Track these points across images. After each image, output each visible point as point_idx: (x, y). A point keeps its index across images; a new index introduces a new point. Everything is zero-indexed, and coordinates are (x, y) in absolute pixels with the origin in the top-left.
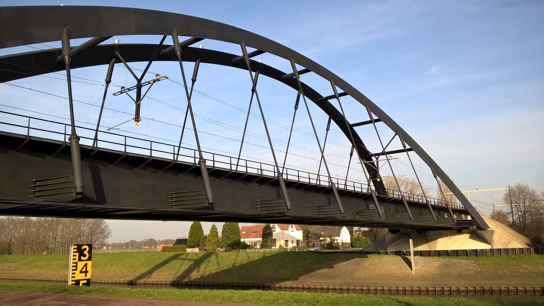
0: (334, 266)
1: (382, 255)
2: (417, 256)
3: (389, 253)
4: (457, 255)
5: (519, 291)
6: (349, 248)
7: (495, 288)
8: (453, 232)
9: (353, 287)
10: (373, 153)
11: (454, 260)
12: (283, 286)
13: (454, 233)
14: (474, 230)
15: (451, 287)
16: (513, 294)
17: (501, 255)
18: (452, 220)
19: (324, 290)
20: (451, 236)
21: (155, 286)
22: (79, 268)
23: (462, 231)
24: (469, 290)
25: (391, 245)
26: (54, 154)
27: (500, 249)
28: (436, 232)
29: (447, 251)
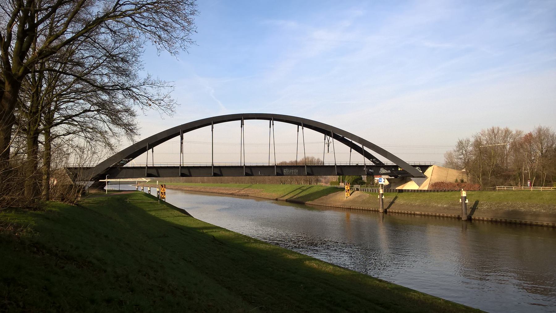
22: (162, 190)
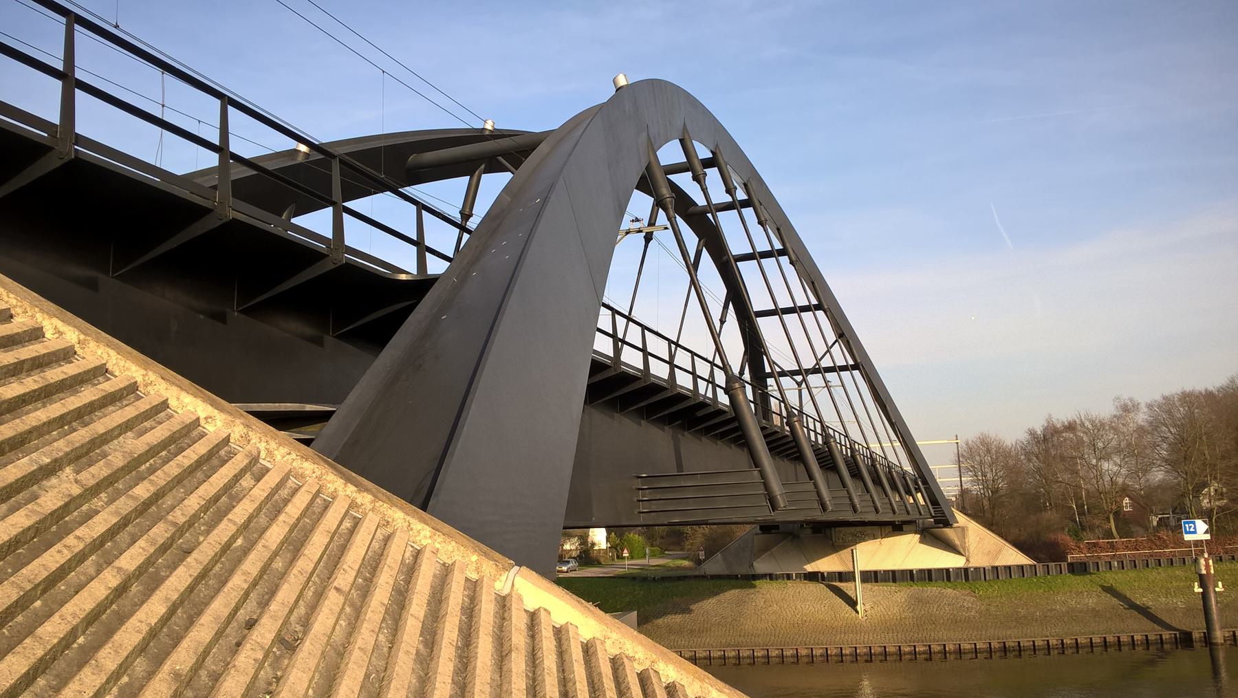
0: (693, 607)
1: (779, 581)
2: (850, 581)
3: (794, 578)
4: (930, 579)
5: (1110, 645)
6: (613, 560)
7: (1025, 643)
8: (885, 531)
9: (777, 652)
10: (786, 370)
11: (931, 590)
13: (887, 532)
14: (926, 526)
15: (753, 650)
16: (1056, 652)
17: (1011, 577)
18: (848, 501)
20: (882, 538)
23: (904, 529)
24: (980, 649)
26: (600, 399)
27: (1009, 567)
28: (852, 529)
29: (911, 571)
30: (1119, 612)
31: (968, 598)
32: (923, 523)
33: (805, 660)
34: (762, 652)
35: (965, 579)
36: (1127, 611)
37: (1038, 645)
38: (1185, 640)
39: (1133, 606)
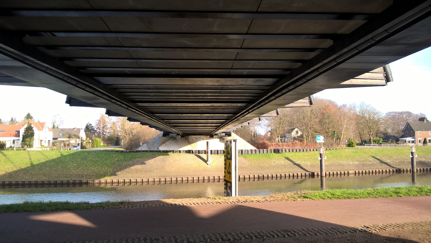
12: (102, 181)
19: (144, 183)
21: (84, 186)
23: (214, 137)
25: (162, 146)
30: (291, 166)
31: (244, 160)
32: (220, 135)
33: (163, 183)
34: (180, 179)
35: (241, 153)
36: (294, 165)
37: (265, 177)
38: (312, 175)
39: (295, 164)
